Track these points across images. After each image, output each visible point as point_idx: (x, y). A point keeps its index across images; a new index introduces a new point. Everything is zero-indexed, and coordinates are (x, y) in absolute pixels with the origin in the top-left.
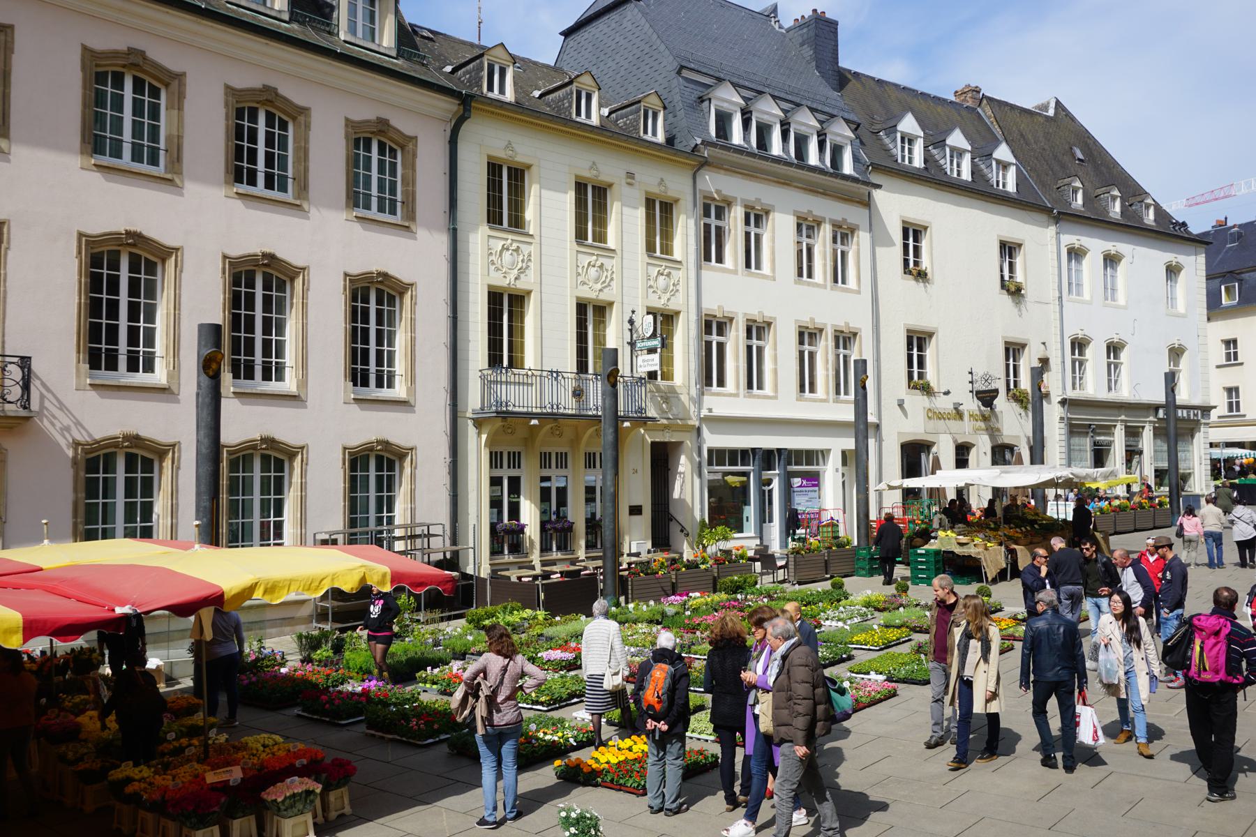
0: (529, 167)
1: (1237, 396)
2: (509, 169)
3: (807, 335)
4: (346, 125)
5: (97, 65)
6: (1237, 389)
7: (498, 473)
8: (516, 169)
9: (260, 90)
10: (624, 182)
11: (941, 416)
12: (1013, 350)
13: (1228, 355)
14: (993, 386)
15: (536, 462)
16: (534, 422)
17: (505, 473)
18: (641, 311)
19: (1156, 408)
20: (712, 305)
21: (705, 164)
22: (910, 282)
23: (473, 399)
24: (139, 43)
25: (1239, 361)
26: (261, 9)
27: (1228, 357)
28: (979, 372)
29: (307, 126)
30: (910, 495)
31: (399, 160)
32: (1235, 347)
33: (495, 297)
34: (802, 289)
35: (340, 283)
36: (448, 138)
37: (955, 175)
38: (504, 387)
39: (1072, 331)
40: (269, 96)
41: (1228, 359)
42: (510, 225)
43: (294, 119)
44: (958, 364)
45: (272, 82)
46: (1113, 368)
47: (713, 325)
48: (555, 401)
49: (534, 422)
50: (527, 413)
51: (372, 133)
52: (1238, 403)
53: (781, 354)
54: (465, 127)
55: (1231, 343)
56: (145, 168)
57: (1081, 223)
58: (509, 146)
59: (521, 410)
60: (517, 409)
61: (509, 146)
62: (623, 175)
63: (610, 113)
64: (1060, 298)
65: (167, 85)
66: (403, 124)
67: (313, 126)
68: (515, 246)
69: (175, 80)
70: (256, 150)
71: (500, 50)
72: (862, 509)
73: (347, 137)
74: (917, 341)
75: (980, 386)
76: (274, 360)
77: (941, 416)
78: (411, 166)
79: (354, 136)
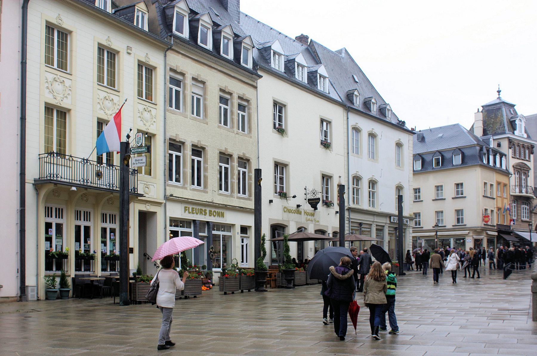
1: (462, 215)
3: (225, 157)
6: (462, 210)
7: (49, 220)
10: (125, 52)
11: (290, 211)
12: (326, 178)
13: (458, 192)
14: (317, 197)
15: (73, 216)
16: (74, 188)
17: (54, 221)
18: (134, 131)
19: (389, 216)
20: (174, 133)
21: (170, 49)
22: (276, 135)
23: (32, 173)
25: (464, 196)
27: (458, 193)
28: (310, 188)
32: (462, 188)
33: (49, 109)
34: (224, 131)
36: (21, 6)
37: (301, 80)
39: (352, 173)
41: (458, 194)
44: (303, 182)
46: (372, 195)
47: (175, 145)
49: (74, 188)
52: (462, 218)
53: (212, 167)
55: (459, 185)
57: (357, 114)
59: (65, 180)
60: (63, 180)
62: (125, 48)
63: (115, 12)
64: (348, 153)
74: (280, 167)
75: (310, 197)
77: (290, 211)
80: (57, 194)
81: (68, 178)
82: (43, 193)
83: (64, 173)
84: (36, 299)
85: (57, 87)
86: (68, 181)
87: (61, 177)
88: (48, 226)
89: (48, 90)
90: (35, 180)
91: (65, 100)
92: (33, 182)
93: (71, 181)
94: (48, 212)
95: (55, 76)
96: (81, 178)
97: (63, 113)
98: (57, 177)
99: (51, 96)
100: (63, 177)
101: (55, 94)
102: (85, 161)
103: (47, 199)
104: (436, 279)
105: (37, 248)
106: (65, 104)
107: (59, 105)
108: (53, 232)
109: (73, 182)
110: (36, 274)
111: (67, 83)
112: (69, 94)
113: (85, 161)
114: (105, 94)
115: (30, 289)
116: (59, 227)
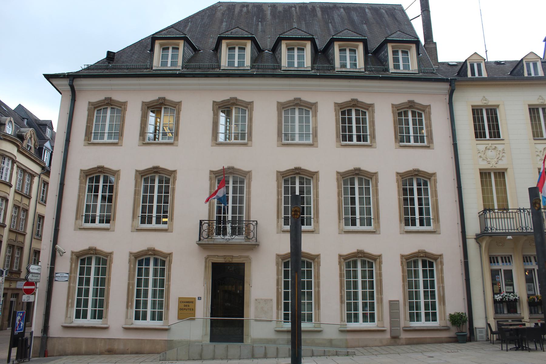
0: (498, 106)
2: (487, 110)
4: (393, 107)
5: (398, 110)
8: (491, 110)
9: (350, 101)
16: (509, 237)
17: (502, 266)
24: (108, 95)
26: (233, 68)
29: (430, 113)
30: (304, 262)
31: (423, 118)
33: (484, 174)
35: (394, 178)
38: (494, 220)
40: (355, 103)
42: (490, 137)
43: (424, 111)
45: (355, 97)
48: (524, 225)
49: (509, 237)
50: (504, 233)
51: (407, 108)
54: (455, 95)
56: (419, 144)
58: (484, 98)
59: (501, 231)
60: (498, 231)
61: (484, 98)
65: (368, 109)
66: (421, 100)
67: (376, 111)
68: (493, 146)
69: (370, 107)
70: (409, 128)
71: (475, 56)
72: (316, 275)
73: (393, 112)
76: (222, 215)
78: (429, 119)
79: (397, 112)
80: (501, 244)
81: (504, 228)
82: (484, 244)
83: (498, 224)
84: (485, 338)
85: (490, 153)
86: (504, 231)
87: (496, 229)
88: (494, 274)
89: (481, 159)
90: (477, 235)
91: (500, 162)
92: (475, 237)
93: (507, 231)
94: (493, 260)
95: (487, 146)
96: (518, 226)
97: (501, 174)
98: (491, 229)
99: (485, 163)
100: (498, 228)
101: (489, 160)
102: (522, 211)
103: (489, 248)
104: (509, 262)
105: (484, 294)
106: (501, 165)
107: (493, 167)
108: (502, 278)
109: (510, 231)
110: (484, 316)
111: (500, 147)
112: (503, 156)
113: (522, 211)
114: (484, 146)
115: (477, 330)
116: (509, 274)
